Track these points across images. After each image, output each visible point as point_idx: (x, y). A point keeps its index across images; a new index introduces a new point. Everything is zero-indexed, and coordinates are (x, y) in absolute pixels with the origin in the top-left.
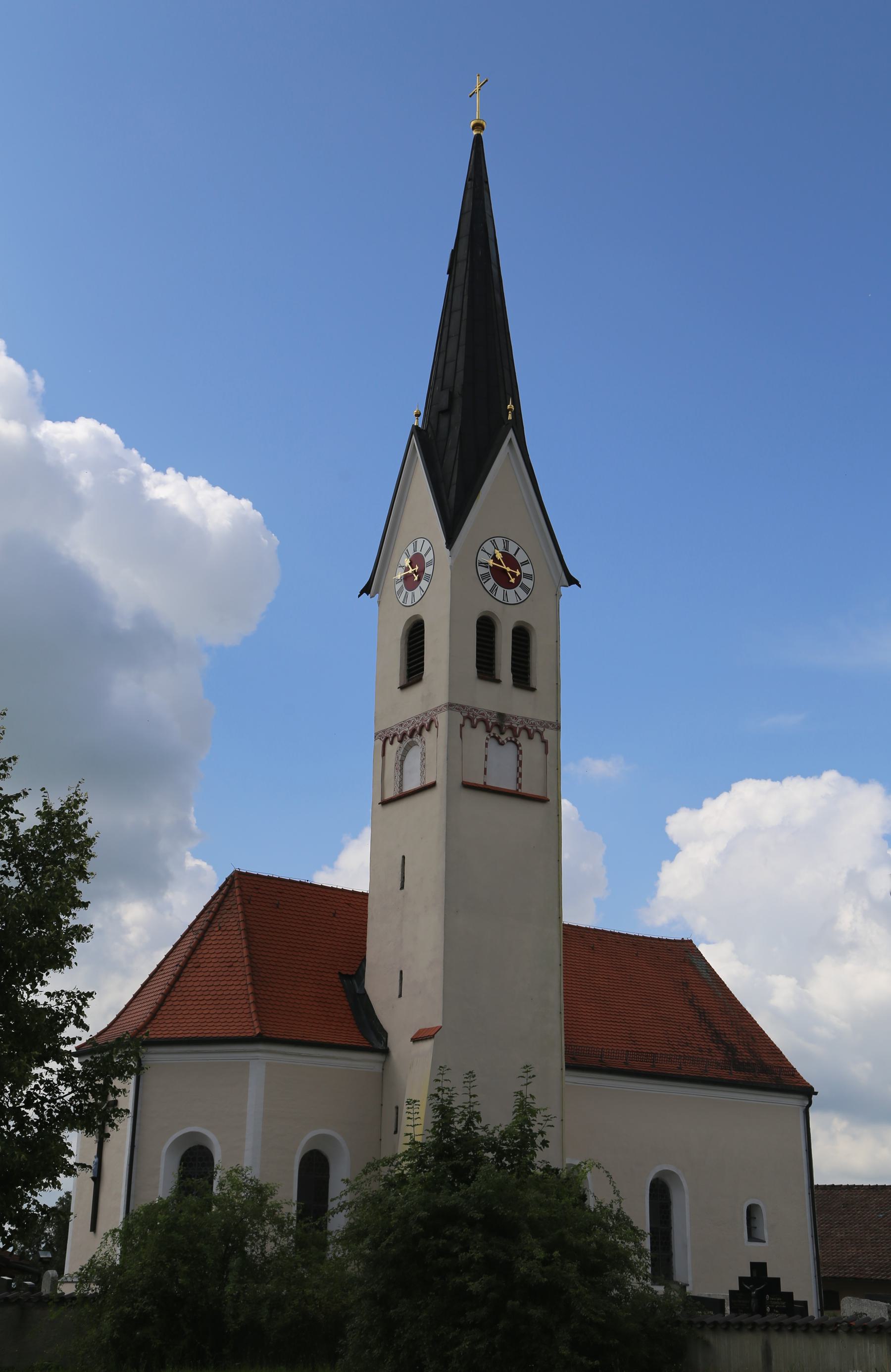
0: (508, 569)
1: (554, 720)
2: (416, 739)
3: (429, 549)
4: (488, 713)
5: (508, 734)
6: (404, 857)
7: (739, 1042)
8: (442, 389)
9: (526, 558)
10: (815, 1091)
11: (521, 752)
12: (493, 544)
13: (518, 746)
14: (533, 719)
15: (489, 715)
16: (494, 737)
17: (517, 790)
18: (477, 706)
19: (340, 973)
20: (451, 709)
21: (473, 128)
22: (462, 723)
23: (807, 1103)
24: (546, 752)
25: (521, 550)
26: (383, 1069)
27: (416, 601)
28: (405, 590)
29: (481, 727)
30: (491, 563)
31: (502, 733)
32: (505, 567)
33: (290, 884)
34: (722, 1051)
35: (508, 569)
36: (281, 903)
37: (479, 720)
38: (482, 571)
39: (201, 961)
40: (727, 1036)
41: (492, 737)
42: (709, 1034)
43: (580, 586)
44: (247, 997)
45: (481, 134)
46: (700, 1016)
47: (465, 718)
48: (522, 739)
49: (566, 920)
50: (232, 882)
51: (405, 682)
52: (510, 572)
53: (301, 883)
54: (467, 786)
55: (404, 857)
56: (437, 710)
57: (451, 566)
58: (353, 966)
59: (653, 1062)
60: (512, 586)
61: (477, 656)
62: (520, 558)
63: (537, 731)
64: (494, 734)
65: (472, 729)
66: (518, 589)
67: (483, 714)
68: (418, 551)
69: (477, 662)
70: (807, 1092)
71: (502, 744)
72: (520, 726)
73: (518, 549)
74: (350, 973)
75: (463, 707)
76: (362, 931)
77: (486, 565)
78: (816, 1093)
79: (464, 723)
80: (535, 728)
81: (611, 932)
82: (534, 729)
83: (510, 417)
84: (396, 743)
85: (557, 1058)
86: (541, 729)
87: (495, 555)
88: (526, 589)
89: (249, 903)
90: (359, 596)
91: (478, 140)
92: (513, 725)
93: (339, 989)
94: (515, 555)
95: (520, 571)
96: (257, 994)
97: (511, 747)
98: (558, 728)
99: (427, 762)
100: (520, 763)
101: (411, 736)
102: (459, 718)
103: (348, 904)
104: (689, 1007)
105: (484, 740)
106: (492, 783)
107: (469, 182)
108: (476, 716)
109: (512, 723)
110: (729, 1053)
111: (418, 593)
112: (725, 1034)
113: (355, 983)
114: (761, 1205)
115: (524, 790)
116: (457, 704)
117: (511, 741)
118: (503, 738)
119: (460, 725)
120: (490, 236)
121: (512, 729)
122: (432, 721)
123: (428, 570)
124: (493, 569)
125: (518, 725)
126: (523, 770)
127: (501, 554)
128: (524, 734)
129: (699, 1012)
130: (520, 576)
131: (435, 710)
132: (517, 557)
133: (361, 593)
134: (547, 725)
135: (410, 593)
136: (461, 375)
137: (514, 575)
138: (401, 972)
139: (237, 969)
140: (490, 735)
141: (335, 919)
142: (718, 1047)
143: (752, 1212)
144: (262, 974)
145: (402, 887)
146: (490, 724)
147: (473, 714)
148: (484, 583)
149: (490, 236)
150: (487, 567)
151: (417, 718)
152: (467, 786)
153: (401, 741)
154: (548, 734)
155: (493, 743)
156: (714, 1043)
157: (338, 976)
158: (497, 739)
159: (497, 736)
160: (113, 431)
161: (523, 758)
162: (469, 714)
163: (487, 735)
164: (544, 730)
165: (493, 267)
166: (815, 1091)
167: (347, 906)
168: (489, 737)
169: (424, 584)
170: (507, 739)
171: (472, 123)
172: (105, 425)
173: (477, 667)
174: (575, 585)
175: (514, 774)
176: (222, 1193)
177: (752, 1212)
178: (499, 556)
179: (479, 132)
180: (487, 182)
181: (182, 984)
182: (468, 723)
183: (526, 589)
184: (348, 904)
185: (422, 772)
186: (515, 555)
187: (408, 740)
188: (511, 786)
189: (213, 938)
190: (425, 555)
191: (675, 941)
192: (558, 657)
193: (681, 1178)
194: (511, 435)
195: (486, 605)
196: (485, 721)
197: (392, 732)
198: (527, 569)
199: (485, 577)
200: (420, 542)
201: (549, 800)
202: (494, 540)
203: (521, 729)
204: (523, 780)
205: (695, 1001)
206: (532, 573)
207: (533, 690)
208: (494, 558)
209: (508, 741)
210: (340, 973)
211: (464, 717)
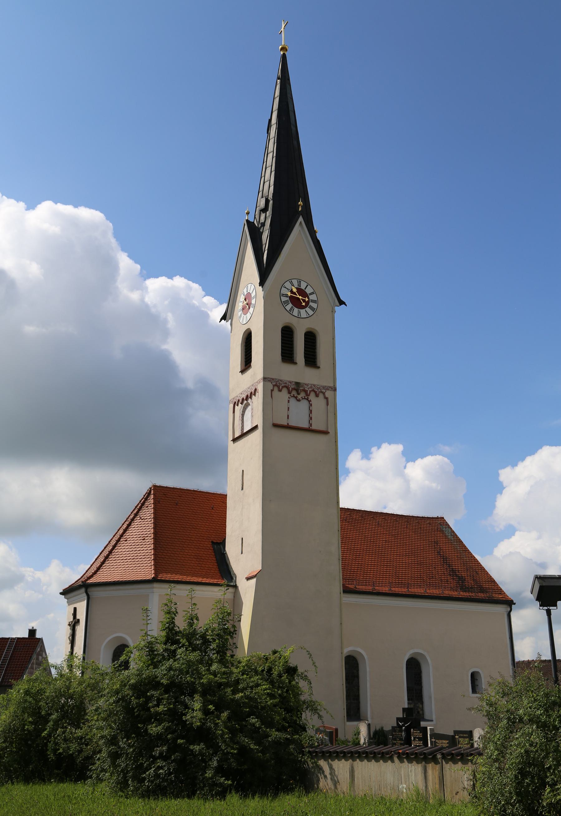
0: (300, 297)
1: (332, 385)
2: (249, 400)
3: (254, 289)
4: (289, 382)
5: (303, 395)
6: (243, 471)
7: (467, 575)
8: (262, 197)
9: (312, 291)
10: (514, 602)
11: (311, 405)
13: (310, 401)
14: (318, 385)
15: (289, 384)
16: (294, 396)
17: (309, 428)
18: (282, 378)
19: (212, 542)
20: (265, 381)
21: (281, 50)
22: (272, 389)
23: (509, 609)
24: (327, 404)
25: (309, 286)
26: (234, 597)
27: (248, 320)
28: (243, 315)
29: (285, 391)
30: (289, 294)
31: (299, 394)
32: (298, 296)
33: (187, 492)
34: (455, 580)
35: (300, 297)
36: (215, 506)
37: (283, 387)
38: (284, 299)
39: (128, 537)
40: (460, 572)
41: (292, 397)
42: (448, 571)
43: (346, 305)
44: (150, 557)
45: (286, 53)
46: (444, 560)
47: (274, 386)
48: (312, 397)
49: (342, 505)
50: (150, 491)
51: (244, 367)
52: (302, 299)
53: (194, 491)
54: (276, 426)
55: (243, 471)
56: (258, 382)
57: (263, 297)
58: (221, 537)
59: (373, 586)
60: (303, 307)
61: (282, 349)
62: (309, 290)
63: (322, 392)
64: (293, 395)
65: (279, 392)
66: (308, 309)
67: (286, 383)
68: (249, 292)
69: (282, 352)
70: (510, 603)
71: (299, 400)
72: (310, 389)
73: (307, 285)
74: (219, 542)
75: (273, 379)
76: (223, 514)
77: (286, 296)
78: (515, 604)
79: (273, 389)
80: (320, 390)
81: (392, 514)
82: (318, 391)
83: (300, 209)
84: (240, 405)
85: (337, 587)
86: (324, 391)
87: (292, 289)
88: (312, 309)
89: (159, 503)
91: (284, 57)
92: (305, 389)
93: (211, 551)
94: (305, 289)
95: (308, 298)
96: (157, 555)
97: (305, 403)
98: (335, 390)
99: (254, 414)
100: (311, 412)
101: (247, 399)
102: (270, 386)
103: (223, 502)
104: (437, 555)
105: (287, 399)
106: (292, 424)
107: (278, 81)
108: (281, 384)
109: (304, 388)
110: (460, 582)
111: (249, 315)
112: (459, 571)
113: (222, 547)
114: (480, 672)
115: (314, 427)
116: (269, 378)
117: (305, 398)
118: (299, 397)
119: (271, 390)
120: (291, 108)
121: (305, 391)
122: (256, 390)
123: (253, 302)
124: (291, 297)
125: (308, 389)
126: (313, 415)
127: (296, 289)
128: (313, 394)
129: (443, 559)
130: (308, 301)
131: (257, 382)
132: (306, 290)
133: (221, 320)
134: (327, 388)
135: (245, 316)
136: (272, 188)
137: (304, 301)
138: (242, 539)
139: (147, 541)
140: (291, 395)
141: (213, 511)
142: (453, 578)
143: (474, 677)
144: (162, 543)
145: (242, 489)
146: (291, 389)
147: (279, 384)
148: (285, 306)
149: (290, 109)
150: (287, 297)
151: (249, 388)
152: (276, 426)
153: (242, 403)
154: (328, 394)
155: (293, 400)
156: (450, 576)
157: (211, 543)
158: (296, 398)
159: (295, 396)
160: (197, 285)
161: (313, 408)
162: (276, 383)
163: (289, 395)
164: (326, 391)
165: (292, 126)
166: (514, 602)
167: (222, 503)
168: (290, 397)
169: (251, 310)
170: (302, 397)
171: (280, 47)
172: (126, 254)
173: (282, 356)
174: (344, 305)
175: (307, 418)
176: (228, 667)
177: (474, 677)
178: (295, 290)
179: (284, 52)
180: (289, 79)
181: (116, 551)
182: (276, 389)
183: (312, 309)
184: (223, 502)
185: (252, 420)
186: (305, 289)
187: (245, 402)
188: (305, 425)
189: (136, 524)
190: (252, 293)
191: (433, 518)
192: (334, 349)
193: (427, 657)
194: (301, 219)
195: (285, 319)
196: (287, 388)
197: (238, 398)
198: (313, 297)
199: (286, 303)
200: (249, 285)
201: (329, 433)
202: (291, 281)
203: (310, 391)
204: (313, 422)
205: (441, 552)
206: (316, 299)
207: (319, 367)
208: (292, 292)
209: (303, 399)
210: (212, 542)
211: (273, 385)
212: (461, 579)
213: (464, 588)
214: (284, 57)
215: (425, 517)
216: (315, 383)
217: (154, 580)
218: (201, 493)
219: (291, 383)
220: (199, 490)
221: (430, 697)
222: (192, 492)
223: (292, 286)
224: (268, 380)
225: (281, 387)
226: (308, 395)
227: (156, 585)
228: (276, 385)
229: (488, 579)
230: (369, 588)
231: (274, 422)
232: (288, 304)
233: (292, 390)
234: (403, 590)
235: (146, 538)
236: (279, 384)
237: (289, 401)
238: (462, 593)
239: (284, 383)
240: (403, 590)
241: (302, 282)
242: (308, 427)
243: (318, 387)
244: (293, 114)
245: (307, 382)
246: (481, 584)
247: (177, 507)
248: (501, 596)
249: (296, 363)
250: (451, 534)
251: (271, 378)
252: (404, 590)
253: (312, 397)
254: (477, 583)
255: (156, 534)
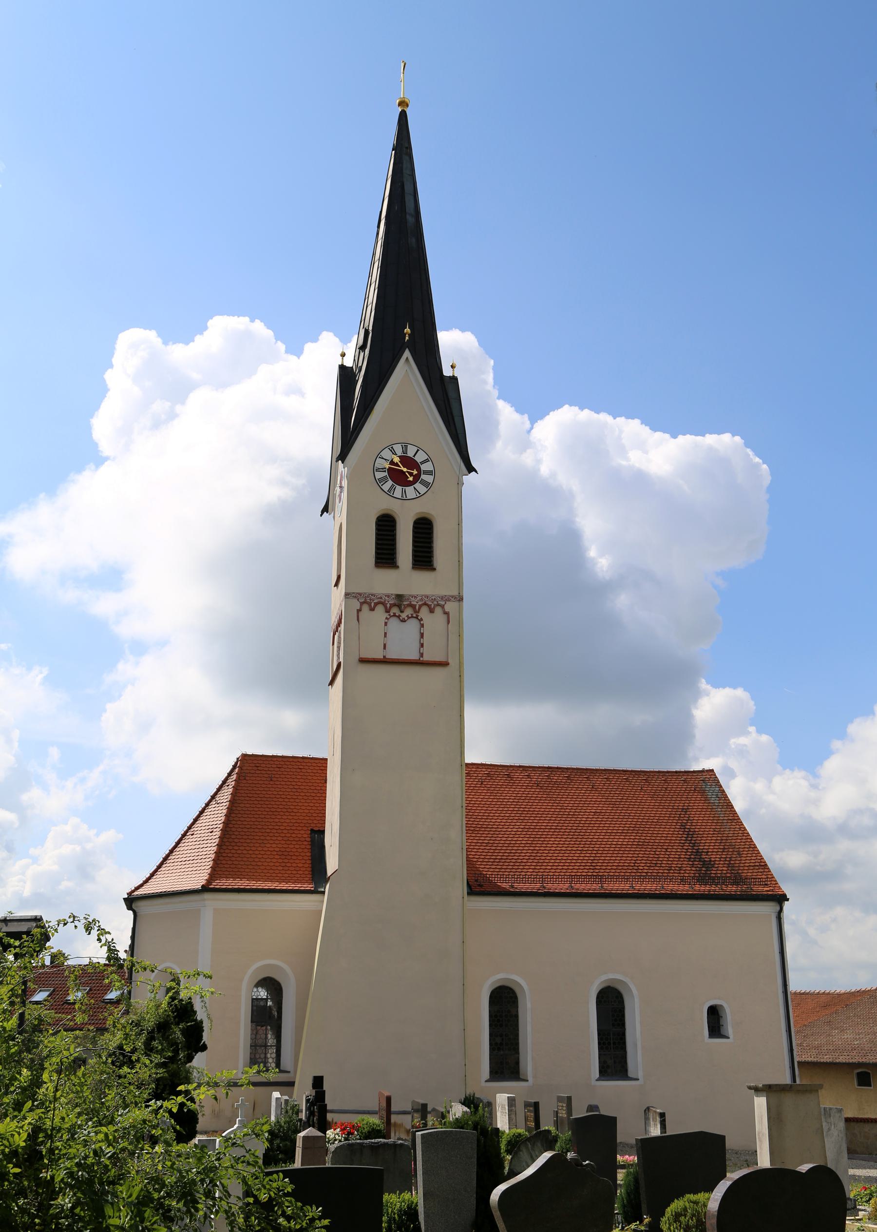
0: (405, 470)
1: (455, 593)
4: (386, 596)
11: (422, 626)
12: (391, 451)
14: (433, 596)
15: (386, 598)
16: (395, 615)
20: (347, 598)
23: (778, 908)
24: (448, 622)
29: (380, 609)
35: (405, 470)
38: (379, 475)
45: (405, 109)
47: (362, 604)
48: (424, 613)
62: (419, 458)
63: (438, 605)
65: (371, 612)
66: (418, 485)
67: (381, 598)
71: (403, 621)
72: (420, 603)
73: (418, 450)
75: (360, 594)
78: (788, 900)
80: (436, 603)
82: (432, 605)
83: (407, 338)
86: (442, 603)
88: (425, 484)
90: (321, 515)
94: (414, 456)
98: (460, 599)
100: (422, 635)
105: (383, 620)
106: (392, 655)
108: (373, 600)
109: (411, 602)
114: (725, 1005)
116: (354, 593)
117: (412, 617)
118: (404, 615)
119: (357, 610)
121: (413, 607)
124: (390, 469)
125: (417, 602)
126: (425, 641)
127: (398, 458)
132: (416, 458)
134: (447, 599)
137: (411, 474)
140: (389, 615)
143: (714, 1013)
147: (370, 600)
150: (385, 471)
155: (393, 622)
158: (399, 617)
163: (387, 615)
164: (446, 603)
170: (407, 616)
177: (714, 1013)
178: (396, 460)
182: (365, 608)
183: (425, 484)
186: (414, 456)
188: (414, 656)
193: (629, 984)
194: (407, 354)
195: (383, 504)
196: (384, 604)
199: (383, 480)
202: (392, 447)
203: (420, 606)
204: (425, 650)
208: (392, 463)
209: (409, 618)
210: (312, 830)
212: (708, 865)
213: (703, 879)
214: (403, 118)
215: (680, 772)
216: (428, 593)
217: (205, 889)
218: (312, 761)
219: (388, 596)
220: (311, 757)
221: (636, 1045)
222: (299, 760)
223: (393, 454)
224: (353, 597)
225: (373, 605)
226: (417, 612)
227: (207, 896)
228: (365, 602)
229: (756, 862)
230: (535, 887)
231: (362, 656)
232: (386, 482)
233: (391, 607)
234: (594, 886)
235: (215, 830)
236: (370, 600)
237: (386, 624)
238: (697, 887)
239: (379, 598)
240: (594, 886)
241: (394, 446)
242: (418, 659)
243: (433, 598)
244: (412, 198)
245: (414, 593)
246: (740, 871)
247: (271, 783)
248: (768, 889)
249: (398, 567)
250: (717, 795)
251: (357, 593)
252: (595, 887)
253: (424, 613)
254: (734, 870)
255: (228, 824)
